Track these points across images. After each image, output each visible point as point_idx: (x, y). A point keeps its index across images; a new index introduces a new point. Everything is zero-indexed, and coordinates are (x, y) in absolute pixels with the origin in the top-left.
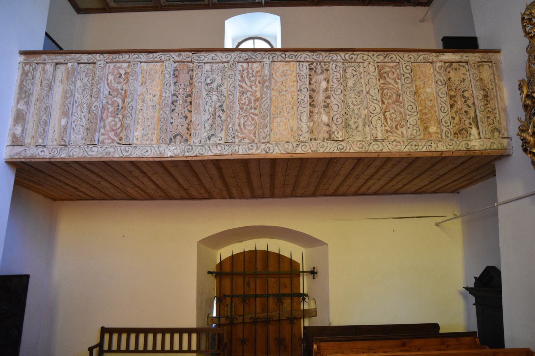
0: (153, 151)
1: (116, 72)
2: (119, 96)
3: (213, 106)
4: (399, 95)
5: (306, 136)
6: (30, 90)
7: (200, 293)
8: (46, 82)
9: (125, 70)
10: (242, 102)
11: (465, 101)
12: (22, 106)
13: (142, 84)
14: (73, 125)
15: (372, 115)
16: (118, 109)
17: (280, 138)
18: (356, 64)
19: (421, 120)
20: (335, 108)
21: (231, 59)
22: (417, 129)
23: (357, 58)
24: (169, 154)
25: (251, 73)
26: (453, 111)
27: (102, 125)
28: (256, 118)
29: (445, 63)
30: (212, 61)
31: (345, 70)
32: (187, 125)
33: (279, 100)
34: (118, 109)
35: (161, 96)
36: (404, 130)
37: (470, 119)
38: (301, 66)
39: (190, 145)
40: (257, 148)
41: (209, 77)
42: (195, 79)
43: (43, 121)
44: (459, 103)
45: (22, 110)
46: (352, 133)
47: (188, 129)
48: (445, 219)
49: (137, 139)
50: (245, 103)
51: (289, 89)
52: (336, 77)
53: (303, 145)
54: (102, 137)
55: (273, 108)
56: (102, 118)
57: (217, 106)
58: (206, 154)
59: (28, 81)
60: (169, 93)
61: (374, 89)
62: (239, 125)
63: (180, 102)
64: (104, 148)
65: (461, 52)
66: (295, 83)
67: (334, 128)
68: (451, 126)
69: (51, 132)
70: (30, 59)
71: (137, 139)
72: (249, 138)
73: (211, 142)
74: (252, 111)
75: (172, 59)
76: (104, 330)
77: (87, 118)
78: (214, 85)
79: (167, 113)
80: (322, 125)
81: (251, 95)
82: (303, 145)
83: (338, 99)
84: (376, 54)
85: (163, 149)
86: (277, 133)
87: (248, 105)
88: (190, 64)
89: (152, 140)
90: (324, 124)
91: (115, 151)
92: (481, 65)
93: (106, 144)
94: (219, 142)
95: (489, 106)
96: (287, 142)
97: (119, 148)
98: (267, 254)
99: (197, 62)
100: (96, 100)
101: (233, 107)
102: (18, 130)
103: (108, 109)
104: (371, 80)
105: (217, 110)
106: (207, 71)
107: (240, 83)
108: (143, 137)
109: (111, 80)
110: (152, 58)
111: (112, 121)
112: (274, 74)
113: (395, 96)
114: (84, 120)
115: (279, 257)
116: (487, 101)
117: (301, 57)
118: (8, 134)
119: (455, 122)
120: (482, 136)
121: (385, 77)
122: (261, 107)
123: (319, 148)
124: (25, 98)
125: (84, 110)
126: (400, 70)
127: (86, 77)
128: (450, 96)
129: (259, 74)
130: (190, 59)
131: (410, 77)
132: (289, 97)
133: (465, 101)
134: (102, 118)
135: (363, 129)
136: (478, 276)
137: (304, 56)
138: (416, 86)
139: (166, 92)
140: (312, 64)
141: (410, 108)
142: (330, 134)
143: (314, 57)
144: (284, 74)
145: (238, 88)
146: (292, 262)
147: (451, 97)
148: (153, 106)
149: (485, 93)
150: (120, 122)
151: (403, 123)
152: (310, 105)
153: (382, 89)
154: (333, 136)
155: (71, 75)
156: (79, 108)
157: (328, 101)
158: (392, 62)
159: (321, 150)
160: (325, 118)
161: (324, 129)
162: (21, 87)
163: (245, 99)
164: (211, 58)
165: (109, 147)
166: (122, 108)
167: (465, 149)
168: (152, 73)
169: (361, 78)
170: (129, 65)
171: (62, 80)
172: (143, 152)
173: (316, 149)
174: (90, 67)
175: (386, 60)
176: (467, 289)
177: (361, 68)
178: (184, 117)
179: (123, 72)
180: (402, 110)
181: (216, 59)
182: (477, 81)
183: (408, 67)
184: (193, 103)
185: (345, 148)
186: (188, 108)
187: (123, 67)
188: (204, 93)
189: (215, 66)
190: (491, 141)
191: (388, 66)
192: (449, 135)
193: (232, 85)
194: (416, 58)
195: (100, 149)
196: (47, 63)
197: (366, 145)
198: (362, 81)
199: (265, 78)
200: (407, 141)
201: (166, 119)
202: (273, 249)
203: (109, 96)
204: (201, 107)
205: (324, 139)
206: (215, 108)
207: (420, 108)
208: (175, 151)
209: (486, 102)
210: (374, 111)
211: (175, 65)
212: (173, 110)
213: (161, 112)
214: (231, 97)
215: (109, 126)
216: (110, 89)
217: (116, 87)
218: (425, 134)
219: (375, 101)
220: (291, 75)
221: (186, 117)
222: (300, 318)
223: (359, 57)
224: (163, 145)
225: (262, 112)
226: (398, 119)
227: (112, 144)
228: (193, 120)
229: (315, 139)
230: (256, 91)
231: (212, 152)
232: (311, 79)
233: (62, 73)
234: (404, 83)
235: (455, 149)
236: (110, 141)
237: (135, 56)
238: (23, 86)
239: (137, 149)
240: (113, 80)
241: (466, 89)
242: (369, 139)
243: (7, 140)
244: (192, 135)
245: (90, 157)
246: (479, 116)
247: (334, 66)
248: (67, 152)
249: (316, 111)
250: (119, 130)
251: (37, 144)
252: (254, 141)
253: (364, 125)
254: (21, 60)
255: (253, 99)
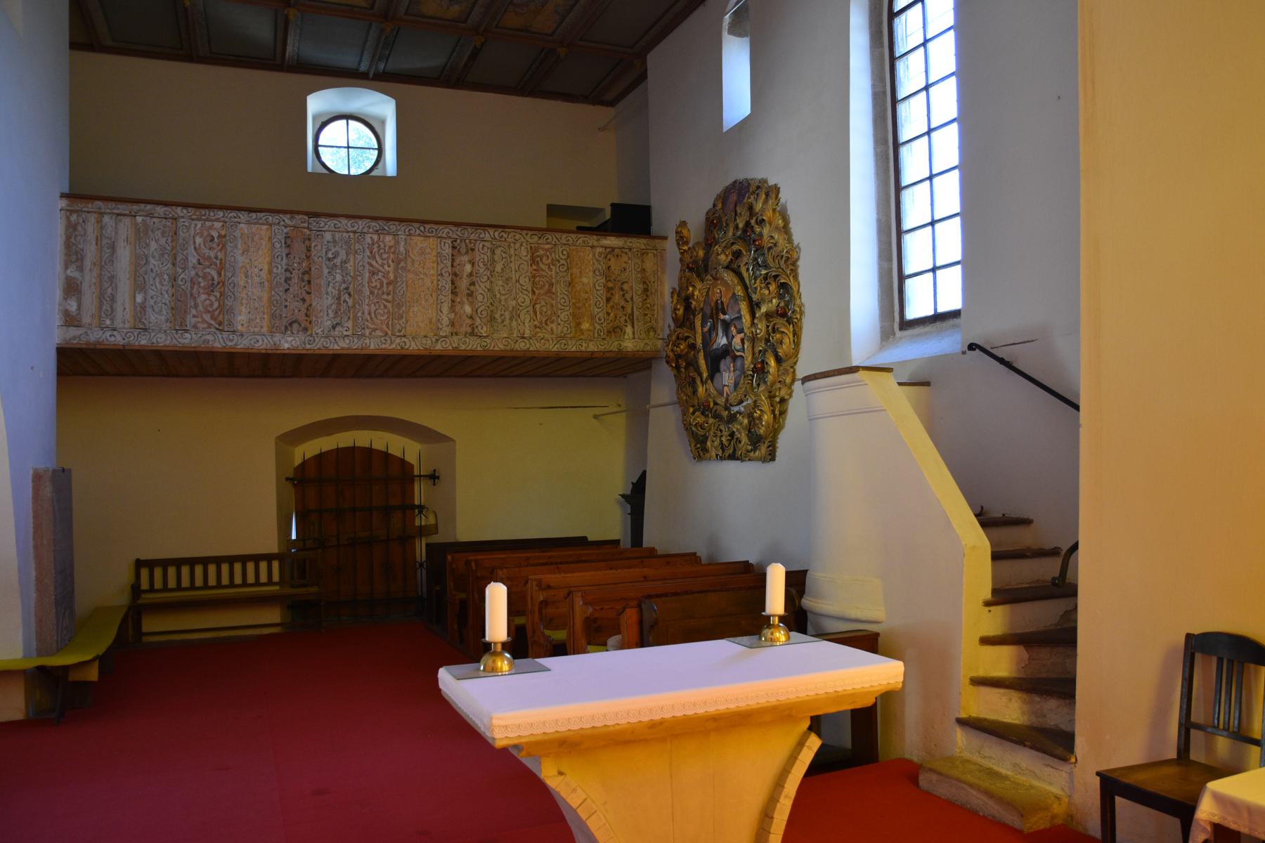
0: (266, 340)
1: (205, 233)
2: (213, 266)
3: (337, 288)
4: (551, 285)
5: (446, 330)
6: (83, 250)
7: (280, 507)
8: (107, 241)
9: (218, 232)
10: (373, 285)
11: (623, 295)
12: (72, 272)
13: (243, 253)
14: (152, 302)
15: (521, 308)
16: (213, 284)
17: (417, 331)
18: (507, 244)
19: (574, 315)
20: (480, 298)
21: (358, 229)
22: (569, 326)
23: (508, 237)
24: (286, 346)
25: (382, 249)
26: (609, 306)
27: (193, 304)
28: (389, 305)
29: (606, 248)
30: (334, 229)
31: (494, 250)
32: (305, 311)
33: (417, 285)
34: (213, 284)
35: (270, 272)
36: (554, 326)
37: (626, 315)
38: (442, 244)
39: (311, 335)
40: (392, 343)
41: (330, 250)
42: (314, 252)
43: (109, 295)
44: (617, 297)
45: (74, 278)
46: (498, 327)
47: (307, 315)
48: (606, 410)
49: (242, 325)
50: (376, 286)
51: (427, 272)
52: (482, 260)
53: (443, 341)
54: (194, 320)
55: (409, 294)
56: (191, 295)
57: (342, 288)
58: (331, 347)
59: (79, 237)
60: (282, 268)
61: (525, 277)
62: (370, 314)
63: (295, 280)
64: (199, 335)
65: (626, 236)
66: (435, 265)
67: (478, 321)
68: (605, 324)
69: (119, 310)
70: (77, 205)
71: (242, 325)
72: (382, 330)
73: (336, 333)
74: (385, 297)
75: (282, 223)
76: (139, 564)
77: (171, 294)
78: (338, 261)
79: (281, 294)
80: (464, 317)
81: (383, 276)
82: (443, 341)
83: (484, 288)
84: (530, 233)
85: (278, 339)
86: (413, 325)
87: (379, 289)
88: (306, 230)
89: (262, 327)
90: (467, 316)
91: (215, 339)
92: (644, 253)
93: (201, 329)
94: (345, 333)
95: (648, 301)
96: (425, 337)
97: (220, 336)
98: (369, 452)
99: (315, 229)
100: (183, 272)
101: (362, 291)
102: (73, 306)
103: (199, 283)
104: (522, 266)
105: (342, 293)
106: (328, 242)
107: (370, 260)
108: (249, 322)
109: (200, 245)
110: (256, 219)
111: (206, 300)
112: (410, 250)
113: (547, 286)
114: (166, 296)
115: (385, 456)
116: (647, 295)
117: (443, 232)
118: (57, 311)
119: (610, 319)
120: (636, 336)
121: (538, 262)
122: (394, 292)
123: (461, 345)
124: (77, 261)
125: (166, 283)
126: (556, 254)
127: (163, 237)
128: (608, 288)
129: (392, 250)
130: (306, 225)
131: (566, 264)
132: (428, 282)
133: (623, 295)
134: (191, 295)
135: (510, 324)
136: (635, 482)
137: (447, 230)
138: (572, 275)
139: (278, 268)
140: (456, 241)
141: (563, 301)
142: (473, 328)
143: (459, 233)
144: (422, 253)
145: (367, 267)
146: (403, 463)
147: (609, 289)
148: (260, 283)
149: (645, 286)
150: (217, 302)
151: (554, 318)
152: (452, 293)
153: (534, 277)
154: (476, 331)
155: (141, 235)
156: (157, 280)
157: (472, 288)
158: (548, 243)
159: (463, 347)
160: (468, 309)
161: (466, 322)
162: (68, 245)
163: (376, 281)
164: (332, 225)
165: (205, 335)
166: (218, 283)
167: (617, 350)
168: (256, 238)
169: (511, 262)
170: (223, 226)
171: (127, 238)
172: (252, 342)
173: (457, 346)
174: (168, 223)
175: (540, 242)
176: (623, 496)
177: (511, 249)
178: (301, 299)
179: (215, 234)
180: (554, 302)
181: (339, 228)
182: (638, 272)
183: (565, 252)
184: (312, 282)
185: (489, 345)
186: (306, 288)
187: (214, 227)
188: (326, 271)
189: (337, 235)
190: (645, 341)
191: (542, 249)
192: (602, 334)
193: (360, 264)
194: (575, 240)
195: (194, 336)
196: (105, 213)
197: (512, 343)
198: (512, 265)
199: (400, 257)
200: (556, 338)
201: (279, 302)
202: (379, 445)
203: (199, 266)
204: (323, 289)
205: (466, 333)
206: (339, 290)
207: (574, 300)
208: (293, 342)
209: (645, 297)
210: (523, 303)
211: (285, 231)
212: (287, 290)
213: (273, 293)
214: (359, 278)
215: (203, 306)
216: (199, 255)
217: (207, 254)
218: (576, 331)
219: (525, 292)
220: (430, 254)
221: (304, 300)
222: (414, 537)
223: (510, 236)
224: (278, 334)
225: (397, 299)
226: (549, 312)
227: (209, 330)
228: (314, 304)
229: (456, 334)
230: (389, 272)
231: (339, 346)
232: (453, 260)
233: (126, 229)
234: (558, 271)
235: (606, 350)
236: (205, 325)
237: (232, 214)
238: (71, 244)
239: (244, 338)
240: (202, 244)
241: (626, 280)
242: (515, 335)
243: (57, 320)
244: (313, 323)
245: (181, 345)
246: (636, 313)
247: (481, 246)
248: (148, 337)
249: (458, 300)
250: (217, 312)
251: (103, 326)
252: (386, 334)
253: (511, 319)
254: (63, 205)
255: (385, 281)
